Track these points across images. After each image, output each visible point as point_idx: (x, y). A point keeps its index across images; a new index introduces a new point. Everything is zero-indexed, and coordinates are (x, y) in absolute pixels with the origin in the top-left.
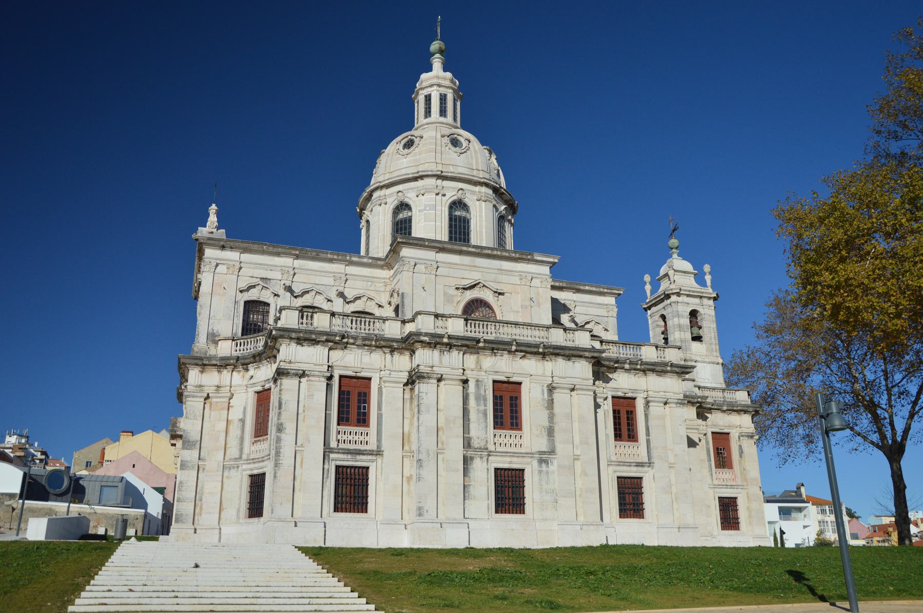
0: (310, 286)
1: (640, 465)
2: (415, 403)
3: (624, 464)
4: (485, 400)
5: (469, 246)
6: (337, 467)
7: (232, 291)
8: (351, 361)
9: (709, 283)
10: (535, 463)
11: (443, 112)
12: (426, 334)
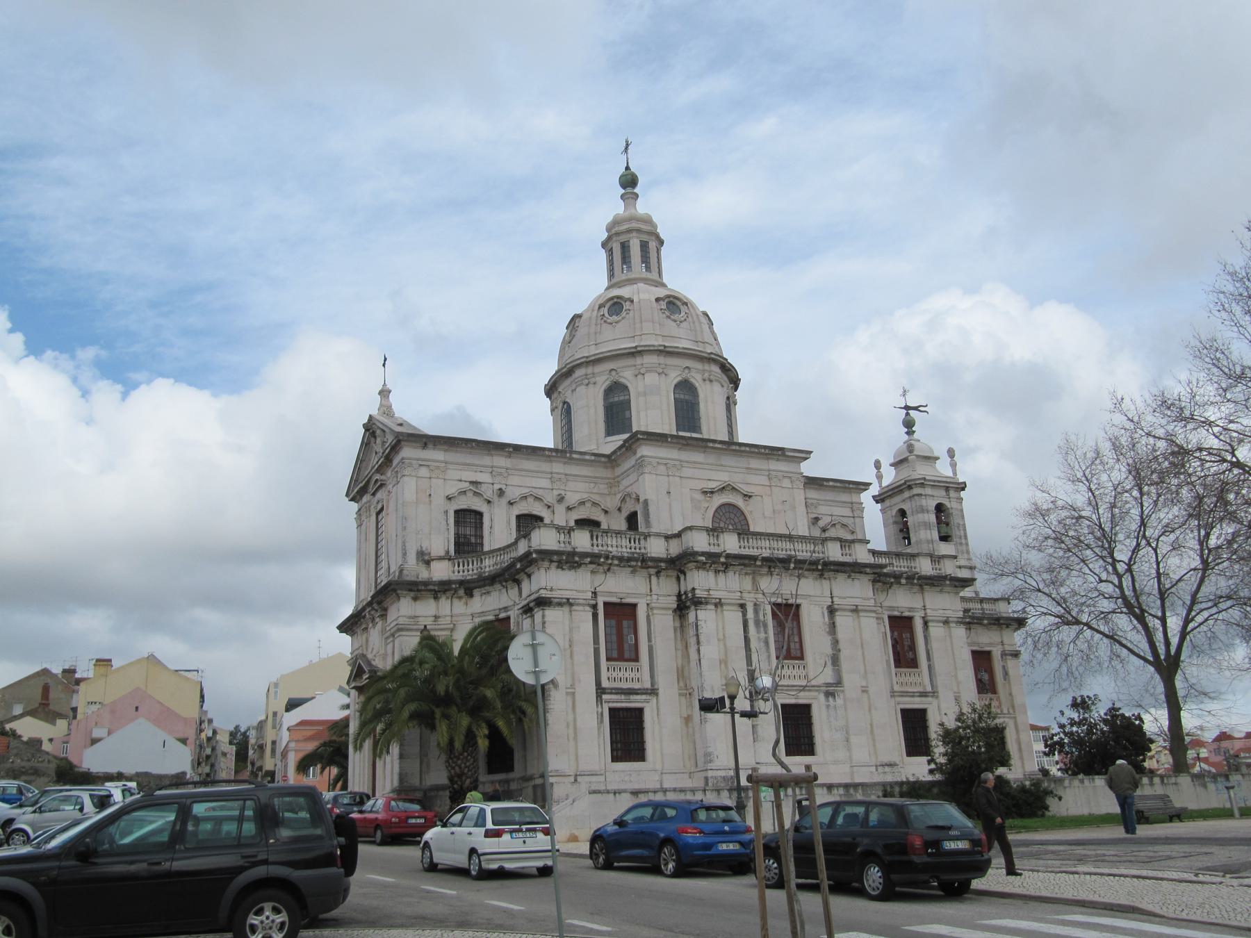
0: (527, 490)
1: (924, 694)
2: (692, 632)
3: (904, 694)
4: (765, 626)
6: (611, 710)
7: (439, 500)
8: (622, 585)
10: (822, 697)
12: (703, 554)
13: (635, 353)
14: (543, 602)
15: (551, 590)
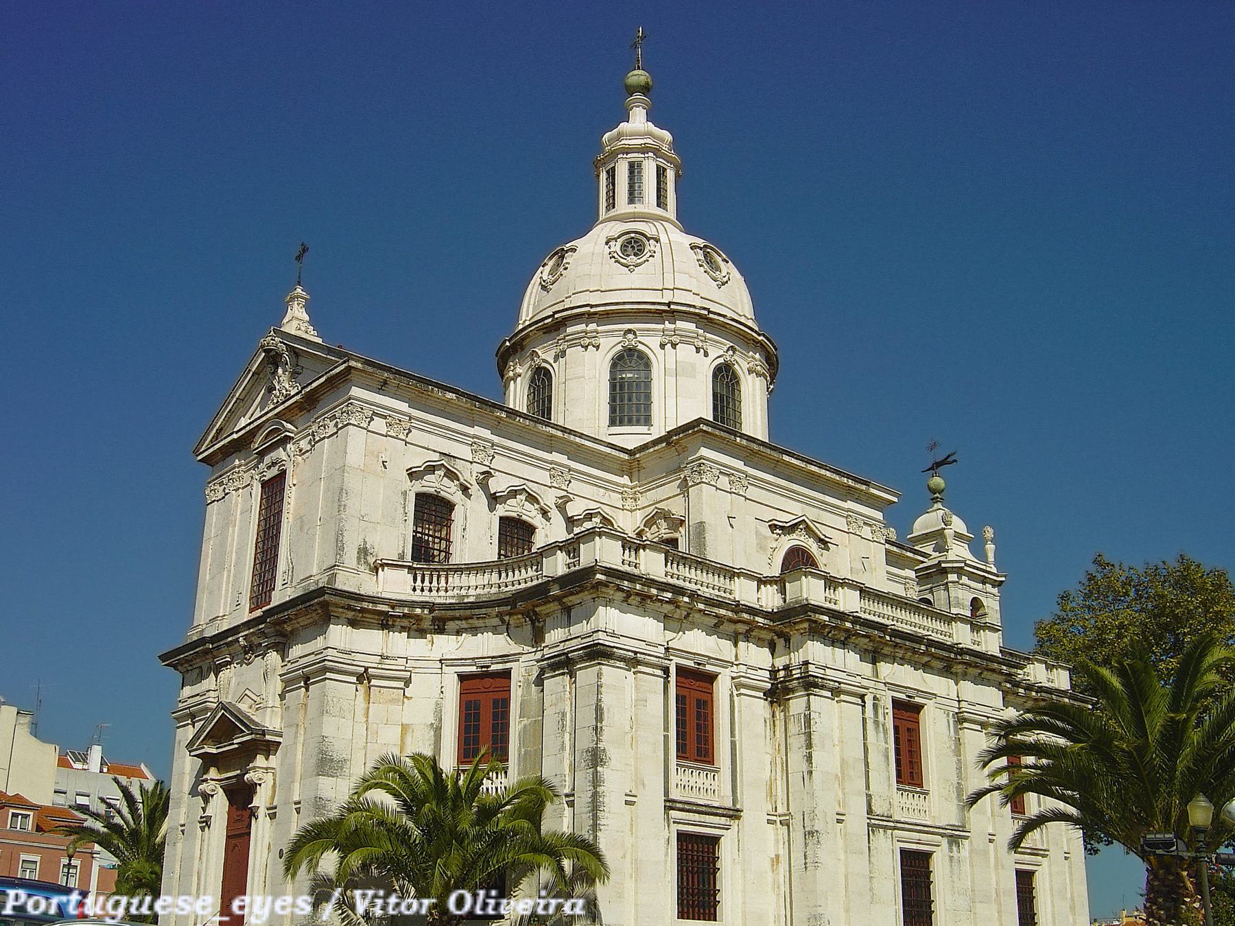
5: (548, 425)
9: (991, 558)
11: (634, 195)
13: (668, 313)
14: (598, 653)
15: (825, 668)
